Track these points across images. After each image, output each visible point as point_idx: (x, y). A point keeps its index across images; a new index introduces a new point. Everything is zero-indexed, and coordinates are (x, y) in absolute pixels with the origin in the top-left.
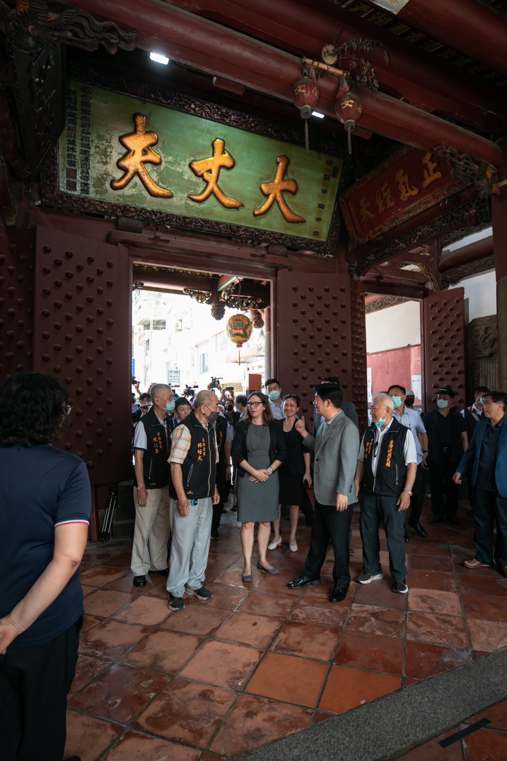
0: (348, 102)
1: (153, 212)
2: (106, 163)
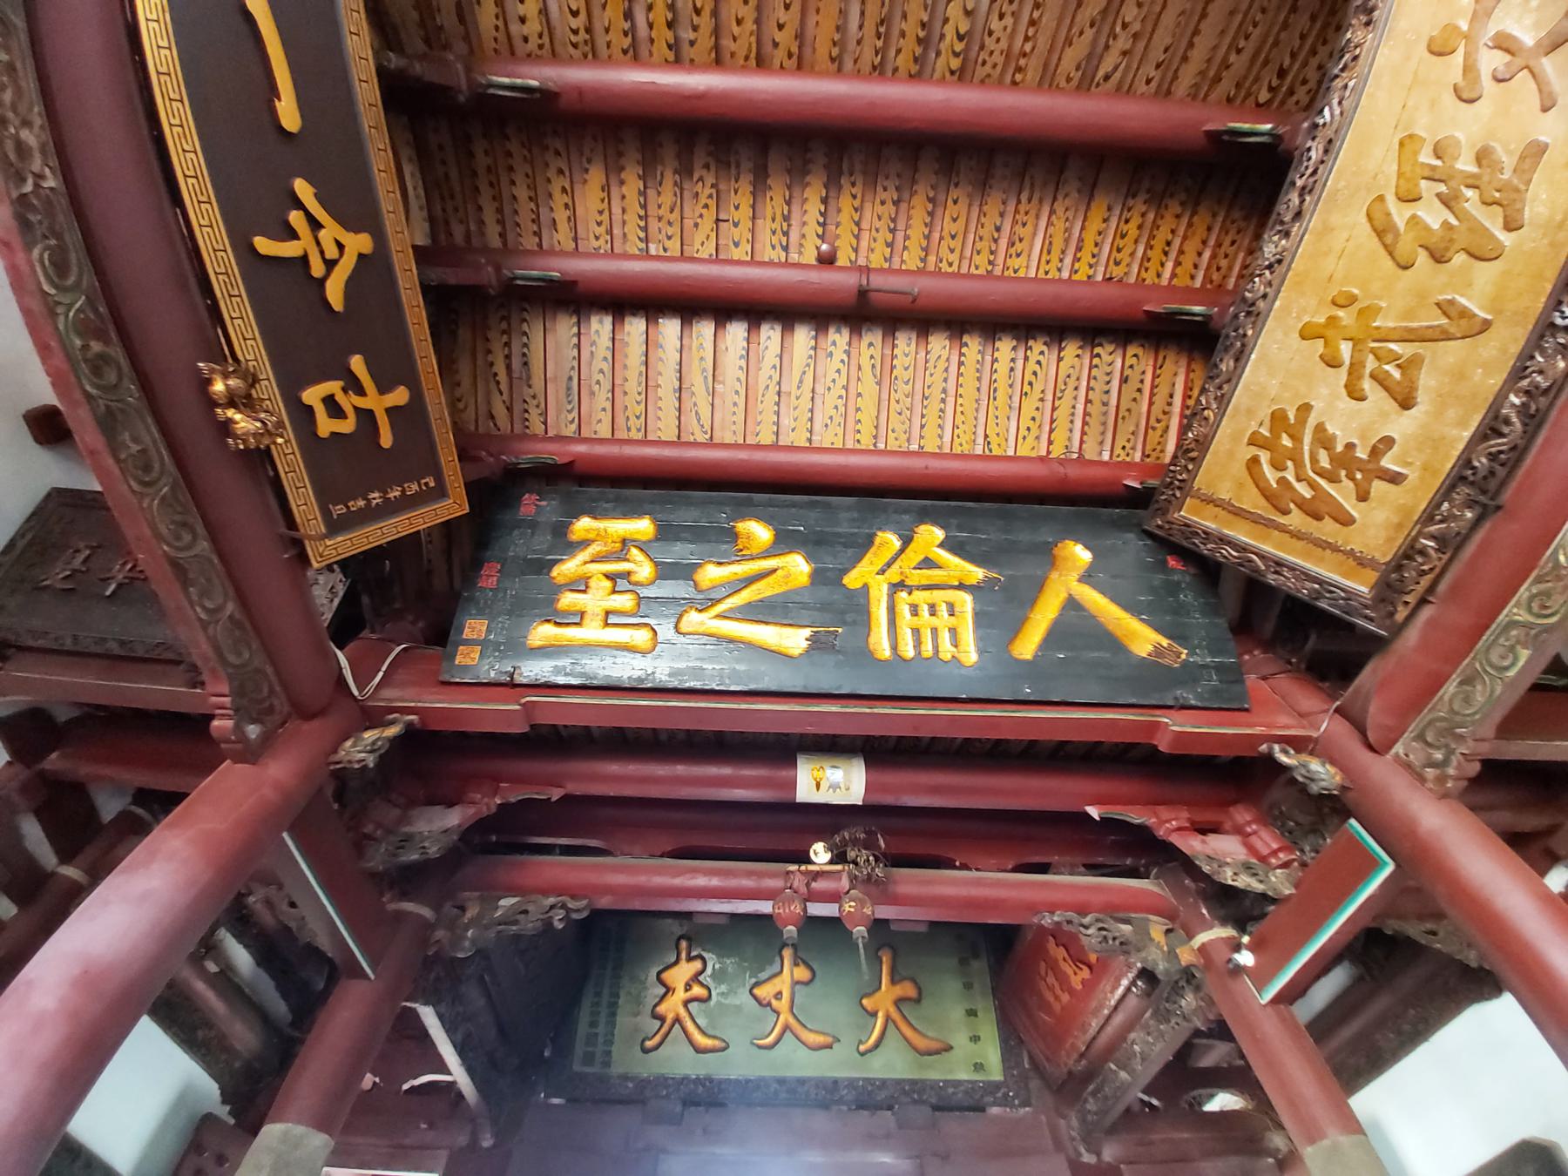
1: (698, 1081)
2: (637, 1014)
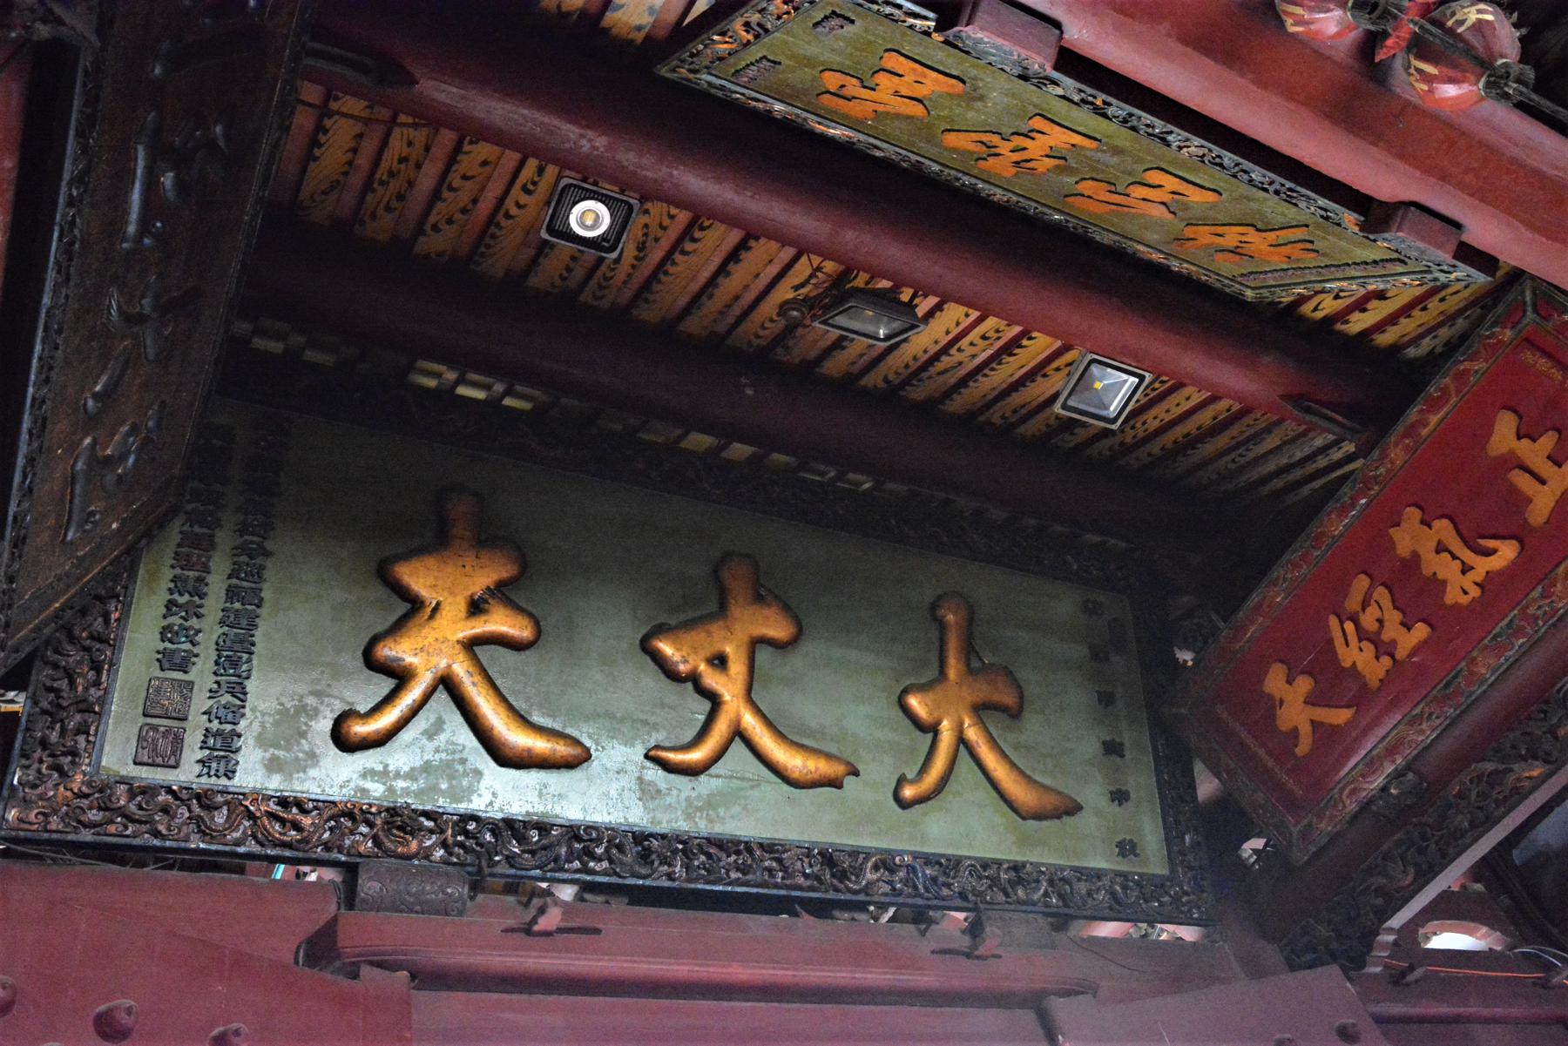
0: (1473, 9)
